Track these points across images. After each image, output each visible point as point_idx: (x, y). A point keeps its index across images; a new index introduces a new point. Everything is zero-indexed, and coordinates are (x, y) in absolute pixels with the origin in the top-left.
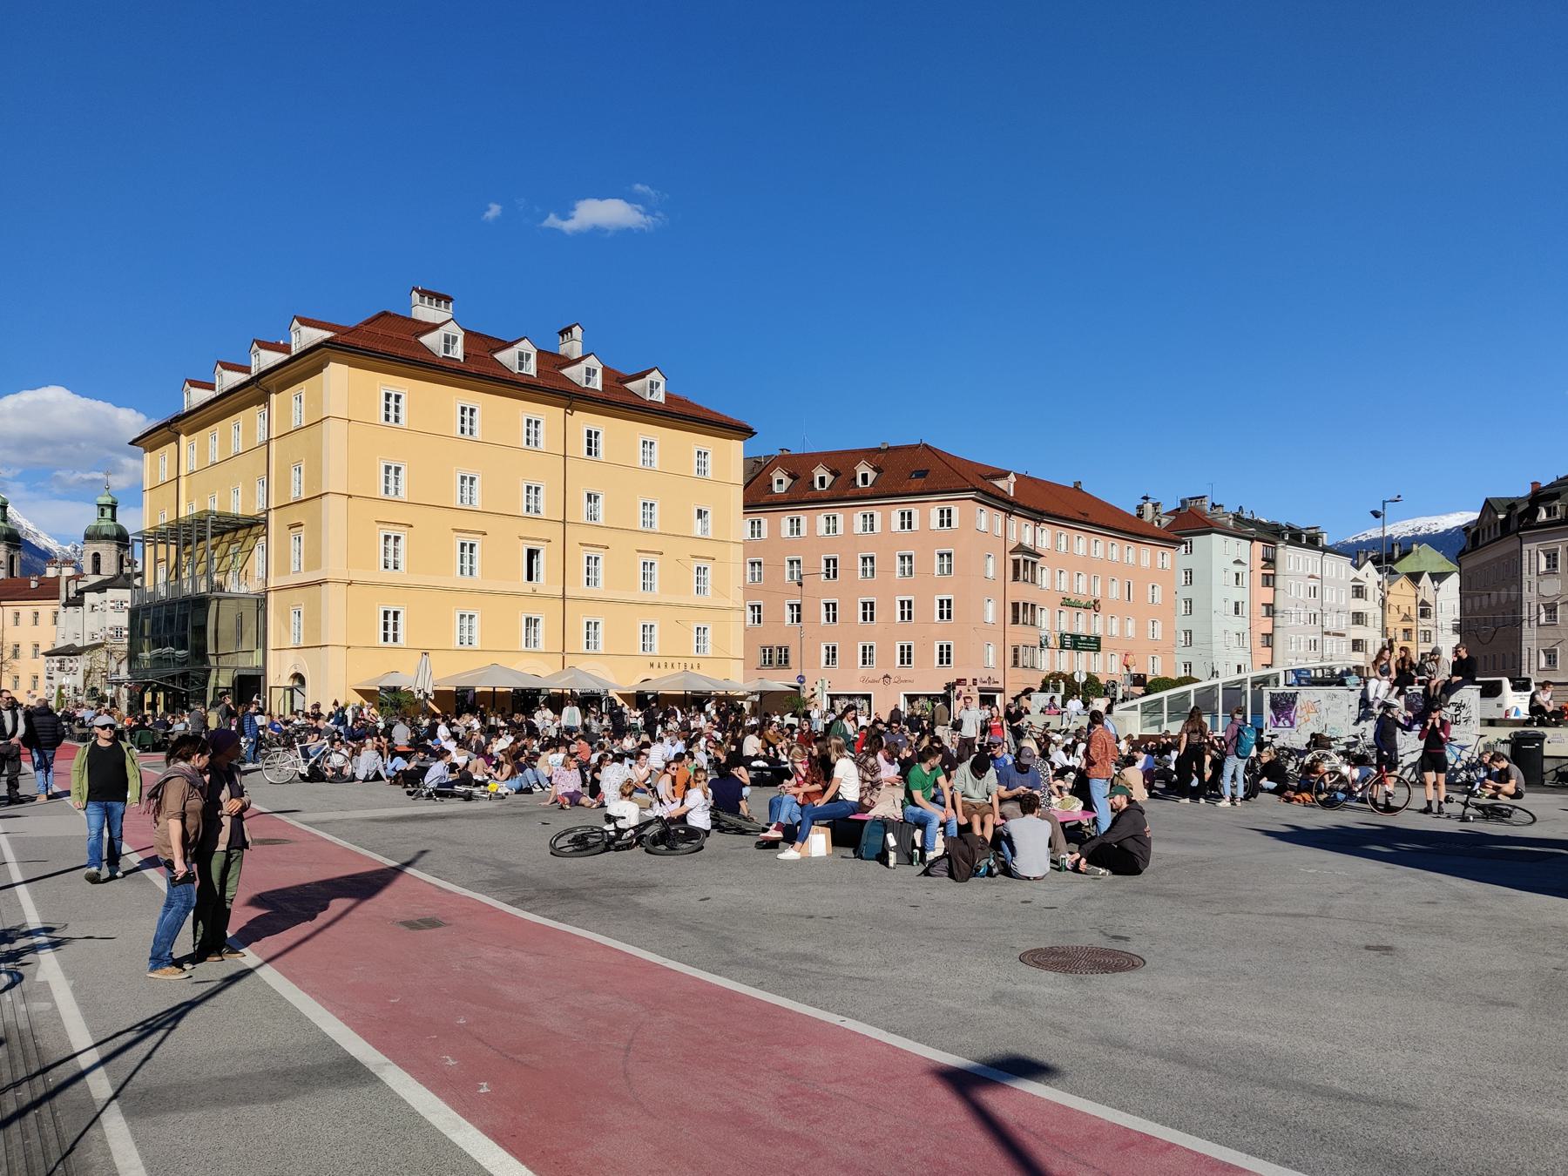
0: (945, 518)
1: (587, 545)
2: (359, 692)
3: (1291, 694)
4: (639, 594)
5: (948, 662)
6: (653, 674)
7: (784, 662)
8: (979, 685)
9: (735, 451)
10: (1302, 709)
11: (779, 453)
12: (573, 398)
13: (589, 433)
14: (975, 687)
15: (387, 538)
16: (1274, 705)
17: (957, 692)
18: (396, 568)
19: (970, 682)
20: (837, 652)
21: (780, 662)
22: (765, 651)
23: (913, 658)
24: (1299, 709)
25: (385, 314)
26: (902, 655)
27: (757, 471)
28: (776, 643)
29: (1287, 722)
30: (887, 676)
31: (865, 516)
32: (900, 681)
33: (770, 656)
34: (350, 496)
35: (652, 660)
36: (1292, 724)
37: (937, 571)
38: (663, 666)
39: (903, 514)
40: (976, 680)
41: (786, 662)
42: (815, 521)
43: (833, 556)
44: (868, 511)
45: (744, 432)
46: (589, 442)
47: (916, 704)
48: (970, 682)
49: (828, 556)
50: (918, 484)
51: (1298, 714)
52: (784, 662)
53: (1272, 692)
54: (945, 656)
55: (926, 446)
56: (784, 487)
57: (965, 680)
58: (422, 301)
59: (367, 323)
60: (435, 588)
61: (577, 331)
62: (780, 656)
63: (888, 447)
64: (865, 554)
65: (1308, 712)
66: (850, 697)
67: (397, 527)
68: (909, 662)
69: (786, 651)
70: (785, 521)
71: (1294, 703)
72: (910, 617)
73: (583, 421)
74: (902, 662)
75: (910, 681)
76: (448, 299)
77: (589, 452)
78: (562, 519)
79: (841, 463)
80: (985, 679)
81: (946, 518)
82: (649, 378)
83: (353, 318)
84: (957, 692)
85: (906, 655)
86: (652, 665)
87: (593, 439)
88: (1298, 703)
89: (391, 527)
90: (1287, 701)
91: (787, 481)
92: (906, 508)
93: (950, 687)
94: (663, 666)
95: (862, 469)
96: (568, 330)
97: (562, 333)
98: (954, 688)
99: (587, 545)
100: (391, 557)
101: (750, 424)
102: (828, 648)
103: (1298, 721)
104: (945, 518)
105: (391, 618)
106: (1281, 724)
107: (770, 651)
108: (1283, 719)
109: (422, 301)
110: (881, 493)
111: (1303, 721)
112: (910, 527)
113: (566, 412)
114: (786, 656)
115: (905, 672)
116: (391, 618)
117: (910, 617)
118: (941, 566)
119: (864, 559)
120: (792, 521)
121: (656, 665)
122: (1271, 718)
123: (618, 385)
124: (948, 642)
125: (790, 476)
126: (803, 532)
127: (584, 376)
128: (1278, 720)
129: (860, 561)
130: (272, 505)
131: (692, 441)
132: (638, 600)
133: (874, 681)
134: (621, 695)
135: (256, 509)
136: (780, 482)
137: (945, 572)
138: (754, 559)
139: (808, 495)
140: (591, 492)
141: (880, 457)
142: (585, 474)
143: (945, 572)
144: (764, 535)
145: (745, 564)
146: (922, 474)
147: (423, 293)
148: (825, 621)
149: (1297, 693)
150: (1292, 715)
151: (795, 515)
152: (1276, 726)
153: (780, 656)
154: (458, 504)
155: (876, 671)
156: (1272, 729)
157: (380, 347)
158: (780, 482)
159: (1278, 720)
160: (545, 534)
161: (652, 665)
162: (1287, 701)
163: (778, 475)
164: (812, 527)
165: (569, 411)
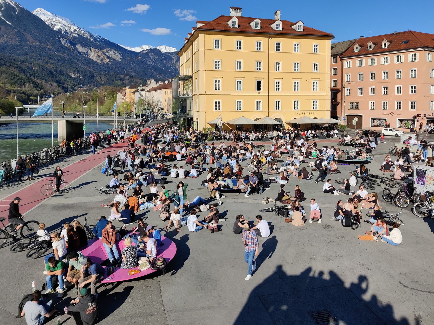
0: (414, 58)
1: (275, 78)
2: (210, 125)
3: (424, 171)
4: (293, 92)
5: (414, 108)
6: (298, 116)
7: (357, 107)
8: (427, 116)
9: (328, 43)
10: (428, 178)
11: (359, 38)
12: (271, 34)
13: (277, 44)
14: (425, 117)
15: (216, 81)
16: (418, 174)
17: (417, 119)
18: (219, 89)
19: (422, 115)
20: (375, 104)
21: (356, 107)
22: (351, 104)
23: (401, 107)
24: (427, 177)
25: (222, 16)
26: (397, 106)
27: (350, 45)
28: (354, 101)
29: (422, 182)
30: (392, 113)
31: (385, 58)
32: (396, 115)
33: (353, 105)
34: (205, 71)
35: (297, 112)
36: (424, 183)
37: (410, 76)
38: (301, 114)
39: (398, 57)
40: (425, 115)
41: (358, 107)
42: (368, 61)
43: (373, 72)
44: (385, 56)
45: (331, 37)
46: (277, 47)
47: (403, 122)
48: (422, 115)
49: (372, 72)
50: (404, 45)
51: (426, 180)
52: (357, 107)
53: (417, 168)
54: (413, 106)
55: (411, 31)
56: (358, 50)
57: (420, 115)
58: (233, 11)
59: (213, 21)
60: (230, 94)
61: (279, 12)
62: (356, 105)
63: (397, 33)
64: (384, 71)
65: (430, 180)
66: (380, 119)
67: (218, 78)
68: (400, 108)
69: (358, 104)
70: (358, 61)
71: (425, 175)
72: (400, 93)
73: (275, 41)
74: (397, 108)
75: (400, 115)
76: (240, 9)
77: (277, 50)
78: (268, 71)
79: (377, 41)
80: (431, 114)
81: (414, 57)
82: (297, 24)
83: (210, 18)
84: (417, 119)
85: (399, 106)
86: (297, 114)
87: (278, 46)
88: (427, 175)
89: (217, 78)
90: (422, 173)
91: (359, 48)
92: (399, 55)
93: (415, 117)
94: (301, 114)
95: (384, 42)
96: (276, 12)
97: (275, 13)
98: (416, 118)
99: (275, 78)
100: (217, 87)
101: (333, 34)
102: (372, 103)
103: (426, 183)
104: (414, 58)
105: (217, 104)
106: (420, 183)
107: (353, 104)
108: (421, 181)
109: (233, 11)
110: (390, 50)
111: (428, 183)
112: (400, 61)
113: (269, 39)
114: (358, 105)
115: (399, 112)
116: (217, 104)
117: (400, 93)
118: (412, 74)
119: (384, 73)
120: (360, 61)
121: (299, 114)
122: (416, 179)
123: (290, 27)
124: (414, 101)
125: (360, 46)
126: (364, 65)
127: (276, 27)
128: (419, 181)
129: (383, 73)
130: (193, 73)
131: (311, 42)
132: (293, 94)
133: (387, 114)
134: (288, 124)
135: (190, 74)
136: (357, 48)
137: (414, 77)
138: (348, 74)
139: (365, 52)
140: (277, 62)
141: (391, 37)
142: (275, 57)
143: (414, 77)
144: (351, 66)
145: (331, 81)
146: (407, 42)
147: (233, 8)
148: (371, 94)
149: (426, 170)
150: (424, 180)
151: (361, 59)
152: (418, 183)
153: (356, 105)
154: (236, 70)
155: (388, 111)
156: (417, 184)
157: (213, 28)
158: (357, 48)
159: (419, 181)
160: (262, 76)
161: (297, 114)
162: (422, 173)
163: (356, 46)
164: (367, 63)
165: (270, 38)
